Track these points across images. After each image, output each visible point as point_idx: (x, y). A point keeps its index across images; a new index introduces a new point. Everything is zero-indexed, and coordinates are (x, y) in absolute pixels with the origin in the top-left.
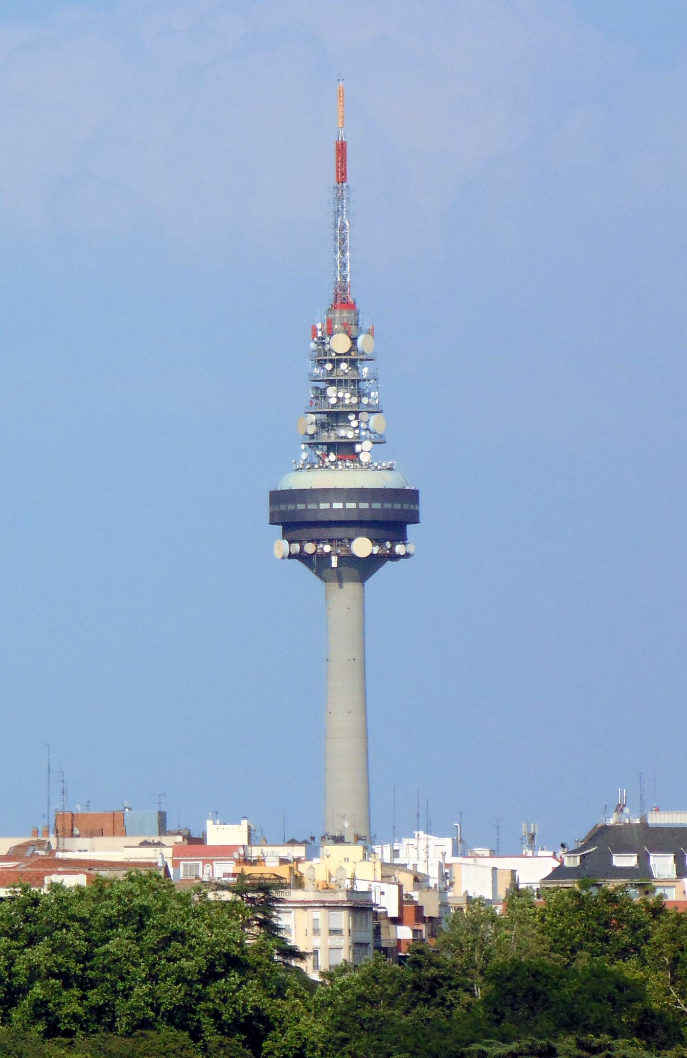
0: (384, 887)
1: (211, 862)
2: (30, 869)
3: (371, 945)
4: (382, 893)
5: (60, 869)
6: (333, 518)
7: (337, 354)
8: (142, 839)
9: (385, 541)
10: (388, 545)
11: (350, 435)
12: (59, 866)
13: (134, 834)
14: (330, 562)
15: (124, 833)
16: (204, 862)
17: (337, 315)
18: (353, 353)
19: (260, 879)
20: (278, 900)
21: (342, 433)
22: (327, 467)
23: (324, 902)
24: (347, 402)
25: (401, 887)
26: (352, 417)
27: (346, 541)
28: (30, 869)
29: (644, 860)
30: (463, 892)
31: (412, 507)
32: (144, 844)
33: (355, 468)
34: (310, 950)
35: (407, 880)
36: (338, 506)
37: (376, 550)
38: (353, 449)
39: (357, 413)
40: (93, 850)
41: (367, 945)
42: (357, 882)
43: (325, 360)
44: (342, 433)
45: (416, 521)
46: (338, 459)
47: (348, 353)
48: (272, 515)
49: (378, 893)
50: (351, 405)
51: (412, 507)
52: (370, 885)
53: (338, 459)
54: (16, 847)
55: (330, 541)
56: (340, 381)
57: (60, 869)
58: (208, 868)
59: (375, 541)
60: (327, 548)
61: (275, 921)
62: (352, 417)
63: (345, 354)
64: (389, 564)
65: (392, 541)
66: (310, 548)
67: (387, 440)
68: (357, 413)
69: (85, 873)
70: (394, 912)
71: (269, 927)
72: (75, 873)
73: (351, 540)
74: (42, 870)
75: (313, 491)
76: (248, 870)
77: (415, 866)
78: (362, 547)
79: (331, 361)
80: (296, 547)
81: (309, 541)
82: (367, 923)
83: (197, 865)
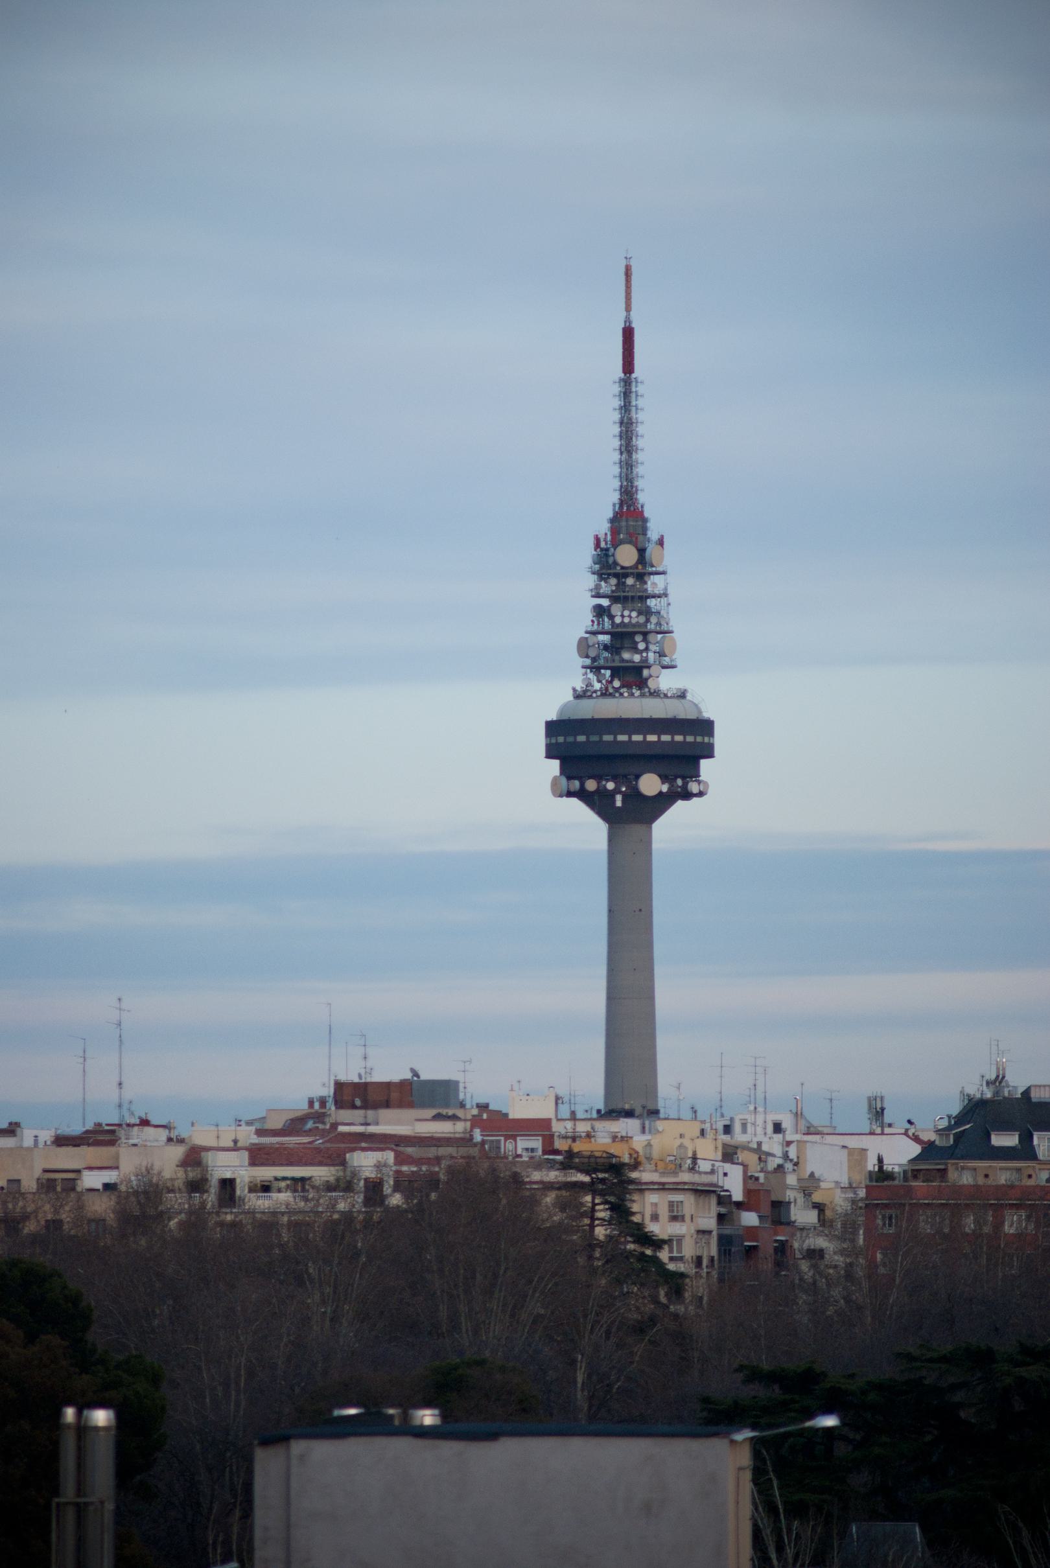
0: (728, 1167)
1: (514, 1137)
2: (329, 1145)
3: (715, 1233)
4: (725, 1174)
5: (364, 1145)
6: (630, 752)
7: (623, 568)
8: (434, 1112)
9: (676, 777)
10: (679, 782)
11: (637, 658)
12: (362, 1141)
13: (423, 1105)
14: (614, 801)
15: (411, 1105)
16: (507, 1137)
17: (624, 524)
18: (640, 567)
19: (589, 1157)
20: (632, 1182)
21: (626, 655)
22: (611, 694)
23: (663, 1184)
24: (634, 621)
25: (745, 1167)
26: (638, 638)
27: (632, 777)
28: (329, 1145)
29: (1026, 1138)
30: (808, 1173)
31: (706, 740)
32: (438, 1117)
33: (642, 695)
34: (666, 1238)
35: (751, 1159)
36: (652, 738)
37: (665, 788)
38: (641, 674)
39: (645, 634)
40: (377, 1124)
41: (710, 1232)
42: (699, 1161)
43: (609, 575)
44: (626, 655)
45: (710, 755)
46: (623, 686)
47: (635, 566)
48: (711, 733)
49: (721, 1174)
50: (638, 625)
51: (706, 740)
52: (713, 1165)
53: (623, 686)
54: (292, 1120)
55: (614, 778)
56: (633, 597)
57: (364, 1145)
58: (510, 1145)
59: (664, 778)
60: (610, 786)
61: (629, 1204)
62: (638, 638)
63: (631, 568)
64: (680, 804)
65: (683, 778)
66: (591, 785)
67: (678, 663)
68: (645, 634)
69: (392, 1150)
70: (738, 1195)
71: (620, 1211)
72: (382, 1150)
73: (638, 777)
74: (343, 1145)
75: (593, 721)
76: (577, 1147)
77: (759, 1144)
78: (650, 784)
79: (616, 575)
80: (576, 784)
81: (590, 778)
82: (709, 1209)
83: (499, 1141)
